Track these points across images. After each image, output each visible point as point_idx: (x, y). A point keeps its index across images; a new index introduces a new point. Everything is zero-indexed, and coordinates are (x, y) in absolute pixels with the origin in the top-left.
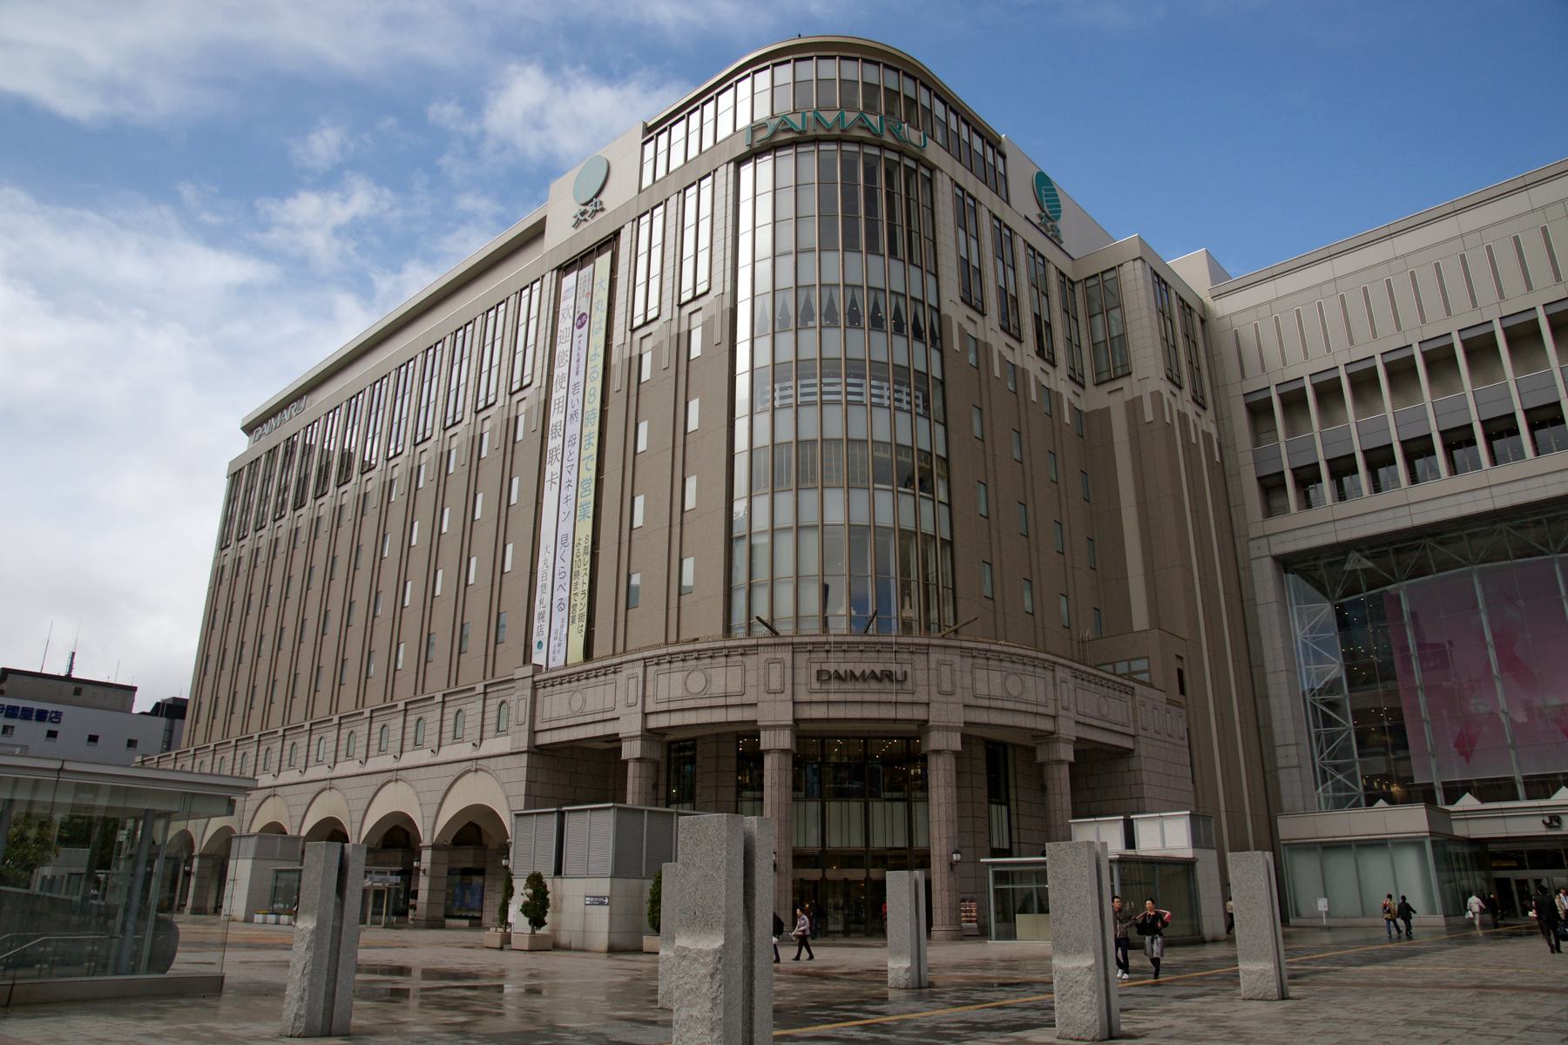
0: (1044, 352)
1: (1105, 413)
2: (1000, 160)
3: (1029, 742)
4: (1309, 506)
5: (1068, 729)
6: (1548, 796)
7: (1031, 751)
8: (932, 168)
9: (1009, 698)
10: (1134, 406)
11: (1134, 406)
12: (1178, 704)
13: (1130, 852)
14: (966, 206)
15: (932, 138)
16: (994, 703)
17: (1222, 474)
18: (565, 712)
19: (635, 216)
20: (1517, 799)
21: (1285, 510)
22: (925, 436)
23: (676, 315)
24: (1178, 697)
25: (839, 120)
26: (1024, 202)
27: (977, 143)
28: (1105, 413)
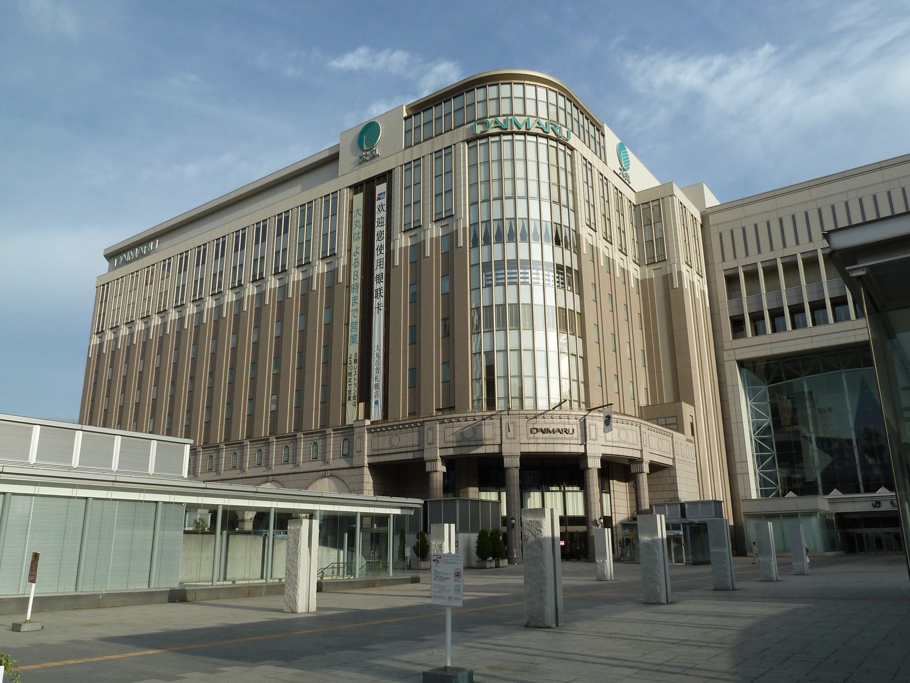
3: (628, 463)
4: (757, 334)
5: (647, 458)
6: (875, 491)
7: (628, 467)
8: (572, 149)
9: (621, 441)
15: (572, 131)
18: (387, 446)
20: (859, 492)
22: (572, 302)
24: (691, 438)
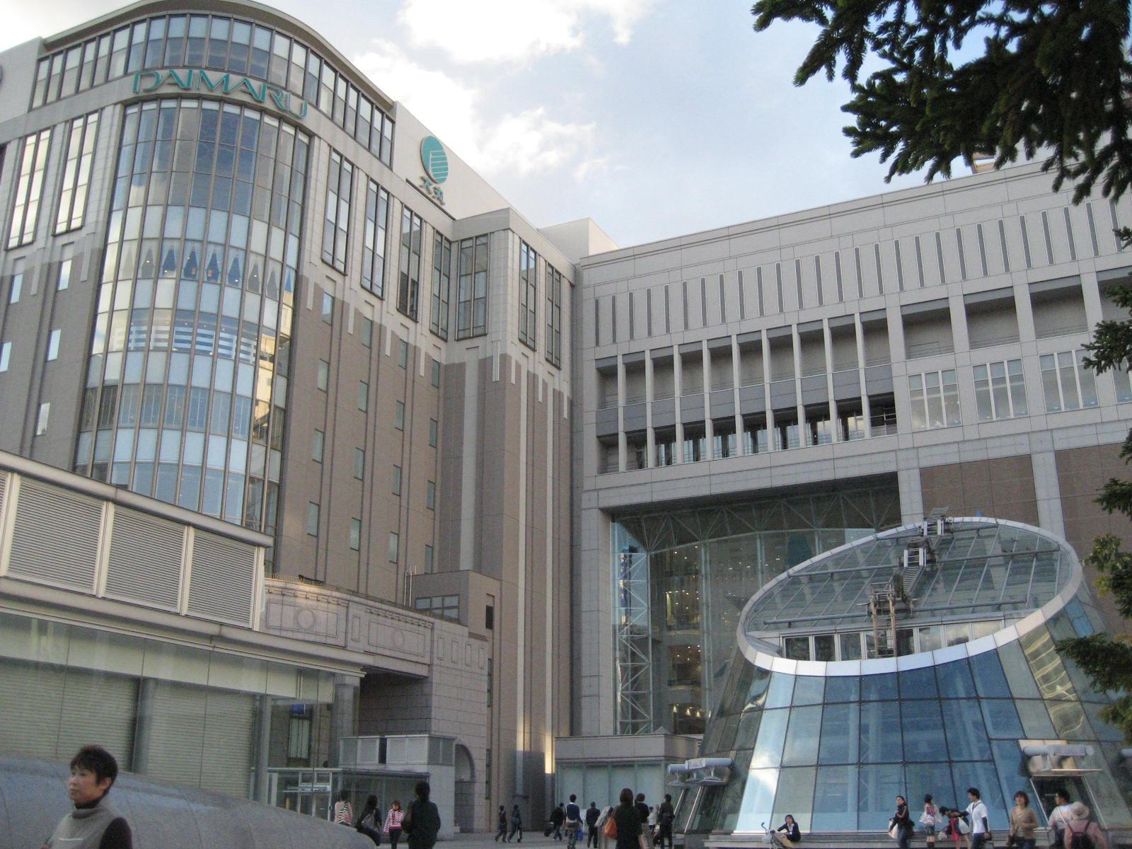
0: (408, 307)
1: (461, 367)
2: (388, 124)
8: (311, 135)
10: (485, 365)
11: (485, 365)
12: (483, 638)
13: (381, 767)
14: (343, 169)
16: (284, 634)
17: (573, 427)
19: (21, 134)
21: (616, 470)
23: (50, 244)
25: (225, 82)
26: (408, 166)
27: (365, 108)
28: (461, 367)
